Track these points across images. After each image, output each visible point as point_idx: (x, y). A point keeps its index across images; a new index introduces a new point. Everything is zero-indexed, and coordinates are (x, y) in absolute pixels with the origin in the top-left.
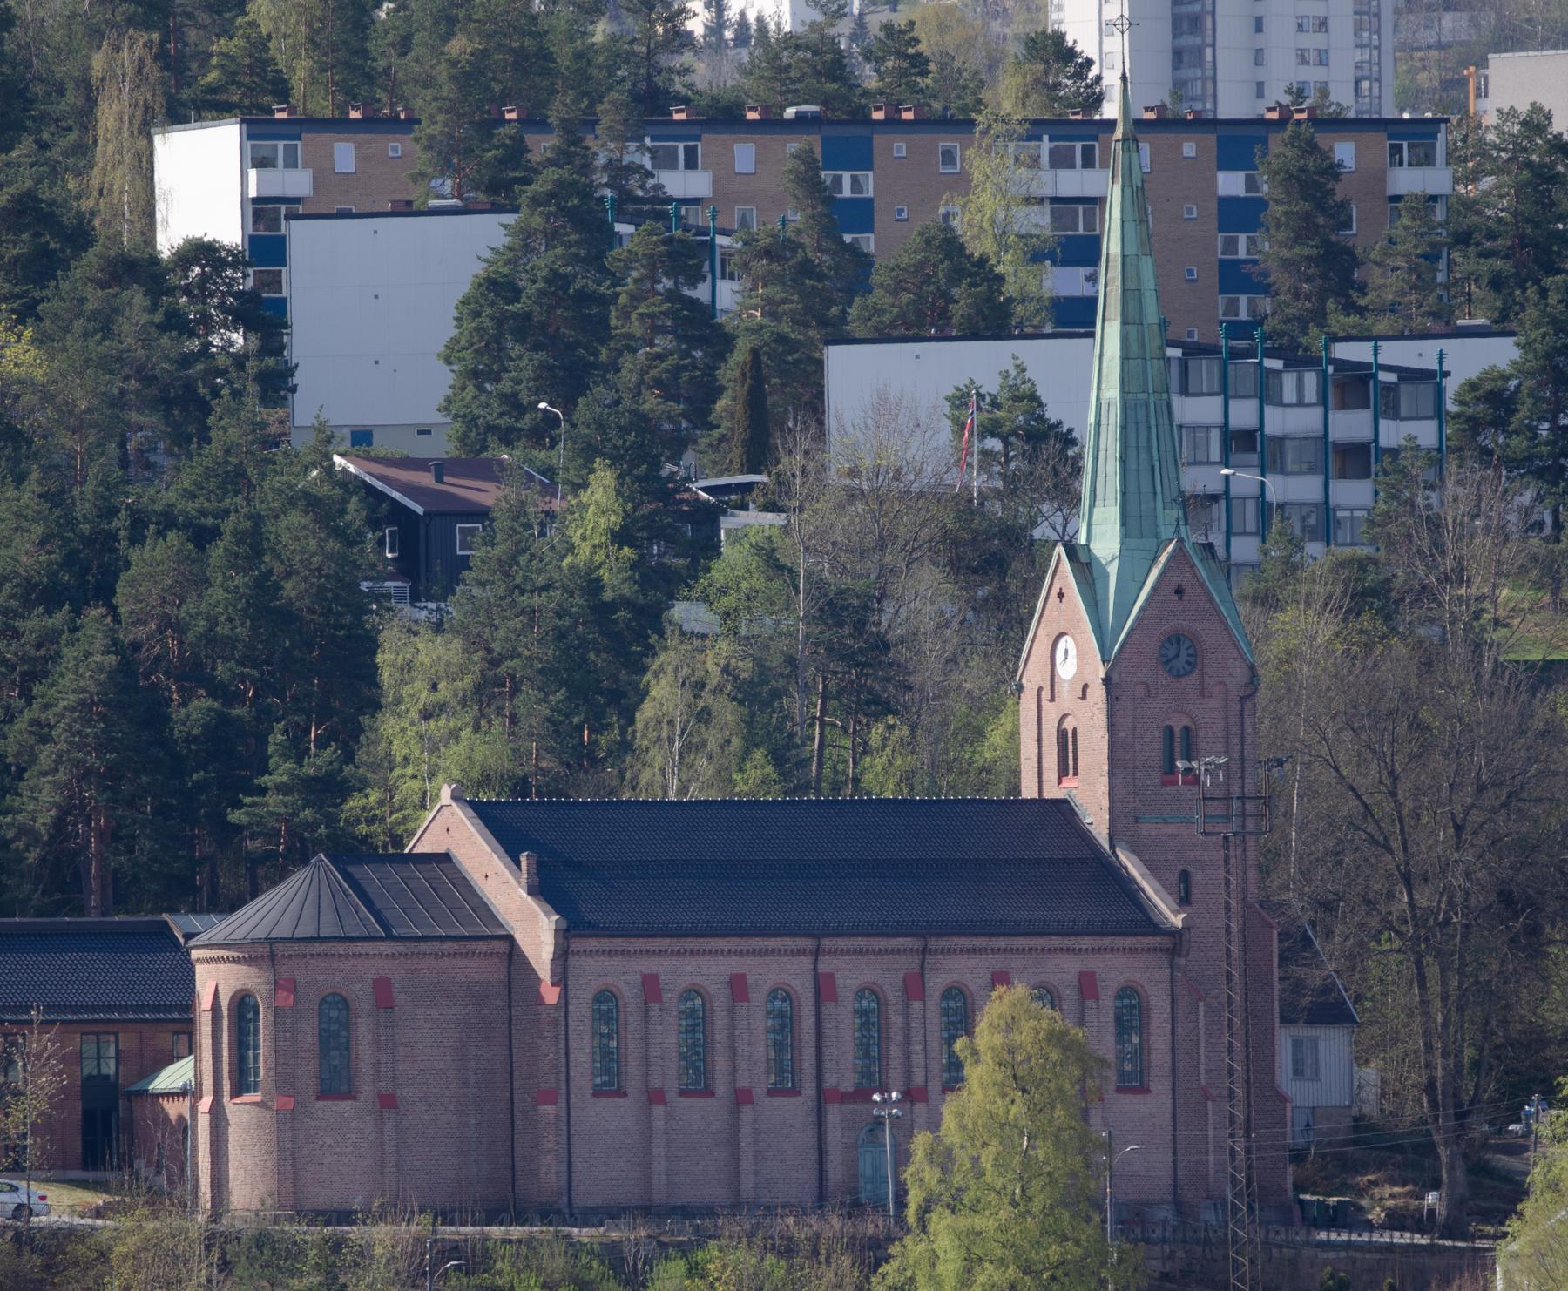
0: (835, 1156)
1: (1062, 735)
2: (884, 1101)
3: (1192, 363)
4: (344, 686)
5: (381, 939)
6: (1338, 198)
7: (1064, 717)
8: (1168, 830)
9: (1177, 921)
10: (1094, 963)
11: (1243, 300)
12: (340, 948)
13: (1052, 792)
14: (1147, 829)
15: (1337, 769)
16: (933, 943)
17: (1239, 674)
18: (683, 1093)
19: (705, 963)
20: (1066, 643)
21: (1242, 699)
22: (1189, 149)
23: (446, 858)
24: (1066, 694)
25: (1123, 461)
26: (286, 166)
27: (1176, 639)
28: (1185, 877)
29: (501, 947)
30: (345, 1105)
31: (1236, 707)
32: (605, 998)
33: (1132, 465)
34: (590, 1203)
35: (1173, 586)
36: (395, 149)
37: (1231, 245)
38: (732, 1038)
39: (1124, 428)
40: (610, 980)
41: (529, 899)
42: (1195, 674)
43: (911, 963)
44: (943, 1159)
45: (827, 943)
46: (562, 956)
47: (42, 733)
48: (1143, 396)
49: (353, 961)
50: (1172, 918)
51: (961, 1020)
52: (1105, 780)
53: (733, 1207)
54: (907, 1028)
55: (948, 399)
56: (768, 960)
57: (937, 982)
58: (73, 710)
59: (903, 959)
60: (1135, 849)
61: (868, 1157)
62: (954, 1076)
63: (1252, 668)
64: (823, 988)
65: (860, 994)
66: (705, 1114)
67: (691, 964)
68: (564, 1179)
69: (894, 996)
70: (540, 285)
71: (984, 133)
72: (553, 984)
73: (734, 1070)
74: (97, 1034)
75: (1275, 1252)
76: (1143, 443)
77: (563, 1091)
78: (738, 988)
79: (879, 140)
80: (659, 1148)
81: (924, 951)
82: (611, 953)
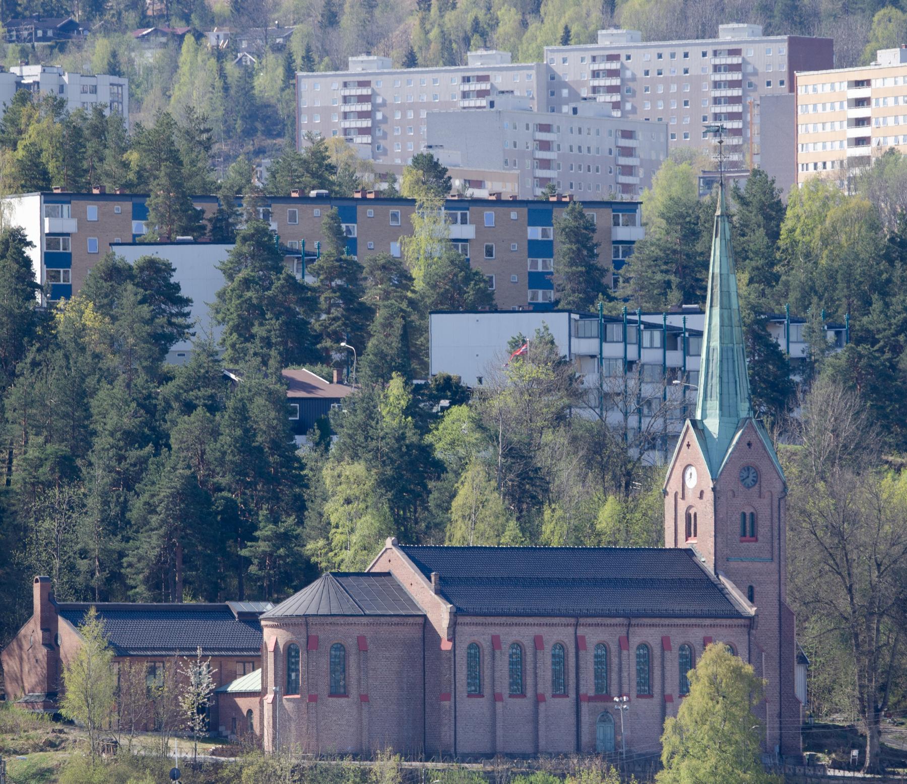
0: (585, 729)
1: (688, 517)
2: (620, 701)
3: (609, 326)
4: (289, 488)
5: (361, 616)
6: (595, 241)
7: (690, 507)
8: (743, 565)
9: (752, 611)
10: (543, 631)
11: (540, 292)
12: (341, 620)
13: (682, 545)
14: (733, 565)
15: (815, 535)
16: (634, 621)
17: (778, 486)
18: (511, 696)
19: (523, 630)
20: (692, 470)
21: (780, 499)
22: (514, 215)
23: (388, 574)
24: (691, 497)
25: (721, 377)
26: (462, 223)
27: (747, 468)
28: (751, 589)
29: (420, 620)
30: (343, 700)
31: (776, 503)
32: (474, 646)
33: (725, 380)
34: (465, 751)
35: (747, 442)
36: (118, 209)
37: (535, 264)
38: (535, 668)
39: (721, 361)
40: (476, 638)
41: (436, 597)
42: (757, 486)
43: (622, 631)
44: (678, 729)
45: (582, 620)
46: (453, 626)
47: (151, 509)
48: (731, 345)
49: (347, 627)
50: (749, 610)
51: (688, 661)
52: (713, 539)
53: (536, 753)
54: (620, 664)
55: (509, 343)
56: (553, 629)
57: (635, 641)
58: (168, 497)
59: (618, 629)
60: (727, 576)
61: (601, 729)
62: (684, 689)
63: (784, 484)
64: (579, 644)
65: (598, 646)
66: (523, 706)
67: (515, 630)
68: (453, 739)
69: (614, 648)
70: (282, 282)
71: (421, 206)
72: (449, 640)
73: (536, 685)
74: (244, 663)
75: (809, 779)
76: (731, 369)
77: (453, 694)
78: (538, 643)
79: (360, 208)
80: (499, 724)
81: (629, 625)
82: (477, 624)
